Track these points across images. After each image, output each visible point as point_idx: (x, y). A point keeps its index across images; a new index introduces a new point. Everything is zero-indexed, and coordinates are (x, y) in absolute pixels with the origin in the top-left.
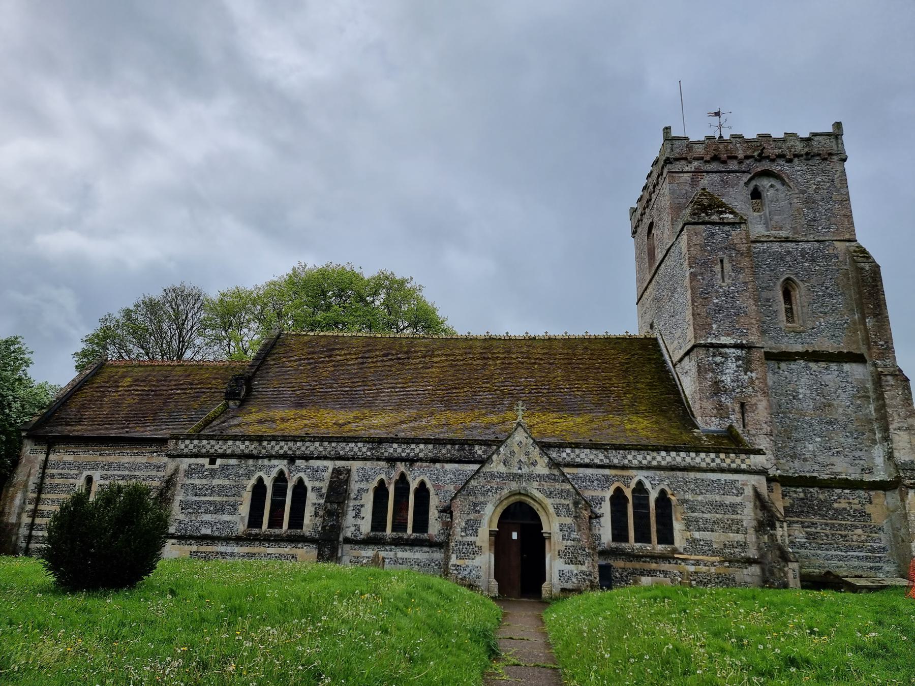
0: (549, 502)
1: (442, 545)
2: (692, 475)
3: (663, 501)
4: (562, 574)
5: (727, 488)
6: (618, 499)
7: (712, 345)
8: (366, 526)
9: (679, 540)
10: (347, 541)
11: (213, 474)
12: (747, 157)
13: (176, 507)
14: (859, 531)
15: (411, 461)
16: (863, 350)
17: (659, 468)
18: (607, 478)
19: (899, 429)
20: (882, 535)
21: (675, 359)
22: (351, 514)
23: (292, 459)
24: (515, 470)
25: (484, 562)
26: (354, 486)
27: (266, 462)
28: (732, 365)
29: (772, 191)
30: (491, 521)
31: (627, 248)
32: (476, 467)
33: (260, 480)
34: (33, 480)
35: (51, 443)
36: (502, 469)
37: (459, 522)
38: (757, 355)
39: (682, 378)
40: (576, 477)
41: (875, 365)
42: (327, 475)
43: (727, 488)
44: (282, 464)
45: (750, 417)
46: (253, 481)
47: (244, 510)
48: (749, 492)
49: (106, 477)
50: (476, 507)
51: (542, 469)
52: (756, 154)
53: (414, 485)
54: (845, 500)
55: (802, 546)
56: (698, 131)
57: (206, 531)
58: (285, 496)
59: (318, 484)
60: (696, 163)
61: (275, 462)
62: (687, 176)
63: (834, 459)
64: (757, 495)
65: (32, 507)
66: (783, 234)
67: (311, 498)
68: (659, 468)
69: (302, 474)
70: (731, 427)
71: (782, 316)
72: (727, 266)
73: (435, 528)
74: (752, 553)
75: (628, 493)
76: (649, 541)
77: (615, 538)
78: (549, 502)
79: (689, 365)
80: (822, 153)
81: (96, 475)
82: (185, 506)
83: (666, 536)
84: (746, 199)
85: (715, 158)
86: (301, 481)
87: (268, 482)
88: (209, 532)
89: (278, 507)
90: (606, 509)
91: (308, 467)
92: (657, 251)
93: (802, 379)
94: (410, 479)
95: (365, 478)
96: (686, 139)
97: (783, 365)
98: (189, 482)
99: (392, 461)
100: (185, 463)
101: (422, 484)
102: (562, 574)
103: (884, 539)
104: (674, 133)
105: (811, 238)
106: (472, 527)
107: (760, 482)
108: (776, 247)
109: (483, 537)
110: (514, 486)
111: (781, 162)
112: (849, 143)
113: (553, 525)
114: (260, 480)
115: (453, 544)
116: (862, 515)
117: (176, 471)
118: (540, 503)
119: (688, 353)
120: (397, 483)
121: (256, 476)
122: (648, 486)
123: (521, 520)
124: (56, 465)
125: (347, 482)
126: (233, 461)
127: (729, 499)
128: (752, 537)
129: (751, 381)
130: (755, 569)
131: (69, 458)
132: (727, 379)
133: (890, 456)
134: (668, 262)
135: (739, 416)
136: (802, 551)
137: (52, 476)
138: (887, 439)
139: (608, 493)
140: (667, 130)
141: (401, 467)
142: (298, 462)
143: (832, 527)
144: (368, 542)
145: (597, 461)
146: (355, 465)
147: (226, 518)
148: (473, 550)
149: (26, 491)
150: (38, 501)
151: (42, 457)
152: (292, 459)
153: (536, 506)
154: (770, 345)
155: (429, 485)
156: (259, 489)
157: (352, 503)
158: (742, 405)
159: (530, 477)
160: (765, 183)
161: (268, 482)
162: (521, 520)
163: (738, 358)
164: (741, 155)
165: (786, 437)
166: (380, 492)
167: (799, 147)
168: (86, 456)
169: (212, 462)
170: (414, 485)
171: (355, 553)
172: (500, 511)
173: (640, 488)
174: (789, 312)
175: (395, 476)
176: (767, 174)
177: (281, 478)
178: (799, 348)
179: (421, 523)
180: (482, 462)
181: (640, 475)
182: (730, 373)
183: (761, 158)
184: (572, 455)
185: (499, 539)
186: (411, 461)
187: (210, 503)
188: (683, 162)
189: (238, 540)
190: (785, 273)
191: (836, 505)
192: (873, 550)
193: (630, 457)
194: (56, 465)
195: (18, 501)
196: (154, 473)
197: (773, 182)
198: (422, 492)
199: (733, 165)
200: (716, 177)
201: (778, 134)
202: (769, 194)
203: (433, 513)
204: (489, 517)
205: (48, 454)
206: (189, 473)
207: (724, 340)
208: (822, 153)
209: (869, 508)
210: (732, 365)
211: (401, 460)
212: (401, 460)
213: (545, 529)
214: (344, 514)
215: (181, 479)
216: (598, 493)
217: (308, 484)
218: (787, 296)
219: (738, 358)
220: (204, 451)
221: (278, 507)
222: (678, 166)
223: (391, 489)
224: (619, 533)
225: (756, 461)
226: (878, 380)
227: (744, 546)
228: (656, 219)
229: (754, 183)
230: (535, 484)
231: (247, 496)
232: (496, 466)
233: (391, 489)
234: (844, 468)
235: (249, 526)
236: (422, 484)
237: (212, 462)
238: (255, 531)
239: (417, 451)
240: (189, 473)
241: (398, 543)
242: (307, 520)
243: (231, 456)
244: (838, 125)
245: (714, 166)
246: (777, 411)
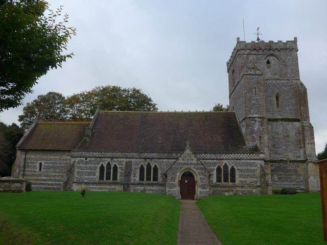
0: (197, 171)
1: (163, 185)
2: (242, 161)
3: (233, 170)
4: (200, 192)
5: (251, 165)
6: (219, 169)
7: (251, 117)
8: (137, 179)
9: (237, 182)
10: (132, 184)
11: (86, 163)
12: (265, 49)
13: (76, 173)
14: (294, 176)
15: (151, 159)
16: (299, 118)
17: (232, 159)
18: (215, 163)
19: (308, 143)
20: (301, 177)
21: (240, 121)
22: (132, 175)
23: (112, 158)
24: (186, 162)
25: (177, 189)
26: (133, 167)
27: (104, 159)
28: (257, 124)
29: (274, 61)
30: (179, 178)
31: (226, 76)
32: (175, 160)
33: (102, 165)
34: (22, 164)
35: (26, 151)
36: (182, 161)
37: (169, 177)
38: (265, 120)
39: (242, 128)
40: (205, 163)
41: (302, 123)
42: (124, 163)
43: (251, 165)
44: (109, 160)
45: (262, 140)
46: (100, 165)
47: (98, 174)
48: (259, 166)
49: (46, 163)
50: (174, 173)
51: (195, 161)
52: (268, 48)
53: (153, 166)
54: (291, 167)
55: (276, 181)
56: (250, 38)
57: (86, 181)
58: (110, 170)
59: (121, 166)
60: (248, 51)
61: (106, 159)
62: (245, 56)
63: (289, 154)
64: (261, 166)
65: (22, 173)
66: (277, 77)
67: (119, 170)
68: (232, 159)
69: (116, 163)
70: (256, 146)
71: (275, 106)
72: (257, 90)
73: (160, 179)
74: (259, 184)
75: (222, 167)
76: (228, 182)
77: (218, 181)
78: (197, 171)
79: (244, 123)
80: (290, 48)
81: (43, 163)
82: (78, 173)
83: (233, 180)
84: (265, 68)
85: (255, 49)
86: (115, 165)
87: (105, 165)
88: (87, 181)
89: (108, 174)
90: (215, 172)
91: (118, 161)
92: (236, 81)
93: (280, 127)
94: (151, 164)
95: (137, 164)
96: (245, 42)
97: (275, 123)
98: (79, 165)
99: (145, 159)
100: (77, 160)
101: (155, 166)
102: (200, 192)
103: (302, 178)
104: (241, 40)
105: (285, 78)
106: (173, 179)
107: (262, 163)
108: (274, 82)
109: (177, 182)
110: (186, 166)
111: (276, 51)
112: (300, 45)
113: (198, 178)
114: (102, 165)
115: (167, 184)
116: (296, 171)
117: (74, 162)
118: (194, 172)
119: (243, 120)
120: (147, 166)
121: (101, 164)
122: (228, 165)
123: (188, 176)
124: (29, 159)
125: (131, 165)
126: (93, 159)
127: (252, 168)
128: (259, 179)
129: (263, 129)
130: (259, 189)
131: (33, 157)
132: (256, 129)
133: (305, 152)
134: (238, 86)
135: (259, 141)
136: (276, 183)
137: (28, 163)
138: (304, 147)
139: (216, 168)
140: (238, 38)
141: (148, 161)
142: (114, 159)
143: (286, 175)
144: (138, 184)
145: (212, 158)
146: (133, 160)
147: (92, 177)
148: (173, 186)
149: (20, 168)
150: (24, 170)
151: (24, 156)
152: (112, 158)
153: (193, 173)
154: (270, 116)
155: (158, 166)
156: (102, 168)
157: (133, 172)
158: (260, 137)
159: (191, 164)
160: (271, 58)
161: (105, 165)
162: (188, 176)
163: (259, 122)
164: (263, 48)
165: (274, 147)
166: (142, 169)
167: (282, 46)
168: (39, 156)
169: (86, 159)
170: (153, 166)
171: (135, 188)
172: (181, 174)
173: (226, 166)
174: (278, 104)
175: (146, 163)
176: (272, 55)
177: (109, 164)
178: (280, 117)
179: (155, 179)
180: (177, 159)
181: (226, 162)
182: (257, 127)
183: (270, 49)
184: (205, 156)
185: (181, 183)
186: (151, 159)
187: (87, 172)
188: (244, 50)
189: (96, 184)
190: (276, 91)
191: (288, 168)
192: (298, 182)
193: (223, 156)
194: (29, 159)
195: (17, 171)
196: (61, 162)
197: (274, 58)
198: (156, 169)
199: (260, 52)
200: (255, 56)
201: (276, 41)
202: (272, 62)
203: (159, 175)
204: (179, 175)
205: (26, 155)
206: (79, 163)
207: (255, 116)
208: (290, 48)
209: (298, 169)
210: (257, 124)
211: (148, 158)
212: (148, 158)
213: (196, 179)
214: (131, 175)
215: (76, 165)
216: (213, 167)
217: (118, 166)
218: (277, 98)
219: (259, 122)
220: (83, 156)
221: (108, 174)
222: (242, 52)
223: (145, 167)
224: (219, 180)
225: (262, 156)
226: (303, 128)
227: (256, 182)
228: (235, 69)
229: (268, 58)
230: (192, 166)
231: (98, 170)
232: (180, 161)
233: (145, 167)
234: (291, 156)
235: (100, 179)
236: (155, 166)
237: (86, 159)
238: (102, 181)
239: (153, 155)
240: (79, 163)
241: (148, 185)
242: (118, 178)
243: (92, 157)
244: (296, 38)
245: (254, 52)
246: (272, 138)
